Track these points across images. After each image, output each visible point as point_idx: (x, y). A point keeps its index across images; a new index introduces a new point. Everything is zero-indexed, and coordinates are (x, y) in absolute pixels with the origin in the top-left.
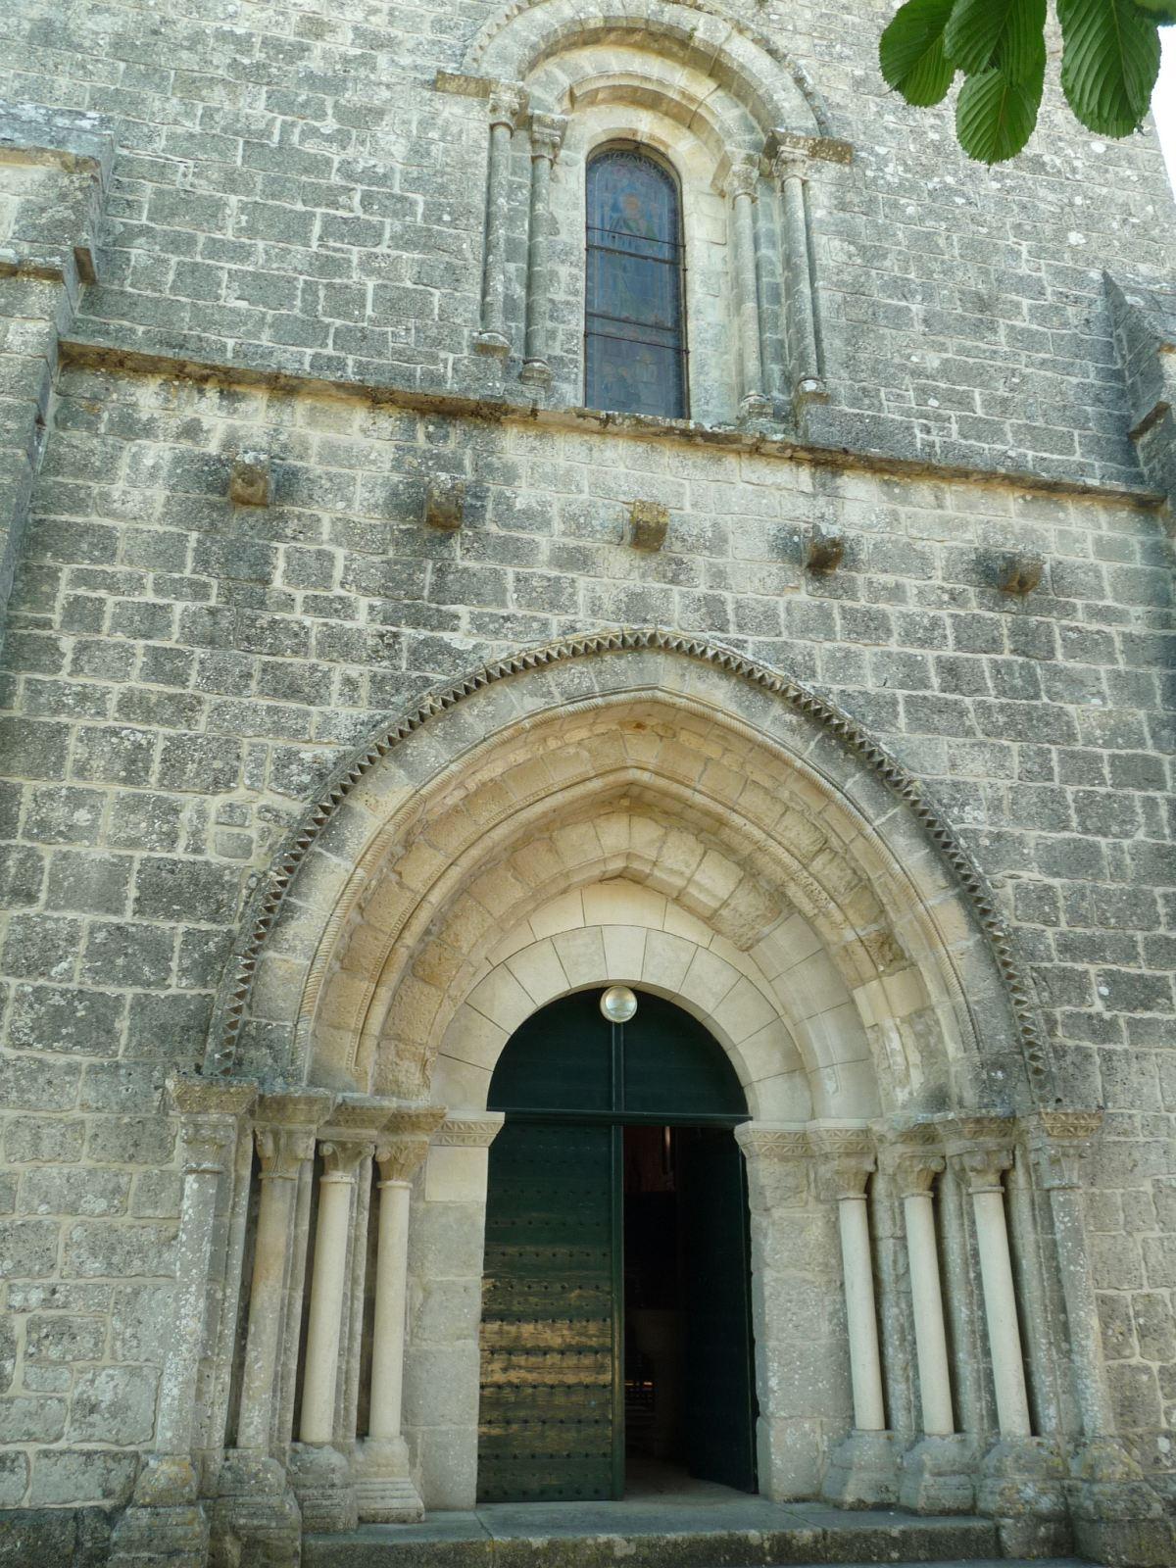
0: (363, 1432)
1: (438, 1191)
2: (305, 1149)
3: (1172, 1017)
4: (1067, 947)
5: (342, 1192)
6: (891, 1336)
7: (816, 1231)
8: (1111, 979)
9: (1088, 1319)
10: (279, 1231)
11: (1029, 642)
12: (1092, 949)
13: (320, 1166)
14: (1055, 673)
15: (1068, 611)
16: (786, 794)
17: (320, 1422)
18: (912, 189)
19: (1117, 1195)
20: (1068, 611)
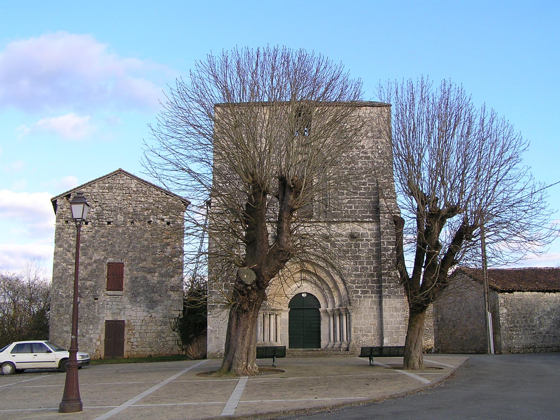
0: (276, 341)
1: (283, 317)
2: (268, 314)
3: (5, 355)
4: (356, 287)
5: (273, 317)
6: (275, 312)
7: (327, 321)
8: (361, 291)
9: (352, 329)
10: (267, 322)
11: (357, 246)
12: (360, 287)
13: (270, 315)
14: (359, 250)
15: (363, 240)
16: (386, 216)
17: (272, 340)
18: (346, 168)
19: (359, 316)
20: (363, 240)
